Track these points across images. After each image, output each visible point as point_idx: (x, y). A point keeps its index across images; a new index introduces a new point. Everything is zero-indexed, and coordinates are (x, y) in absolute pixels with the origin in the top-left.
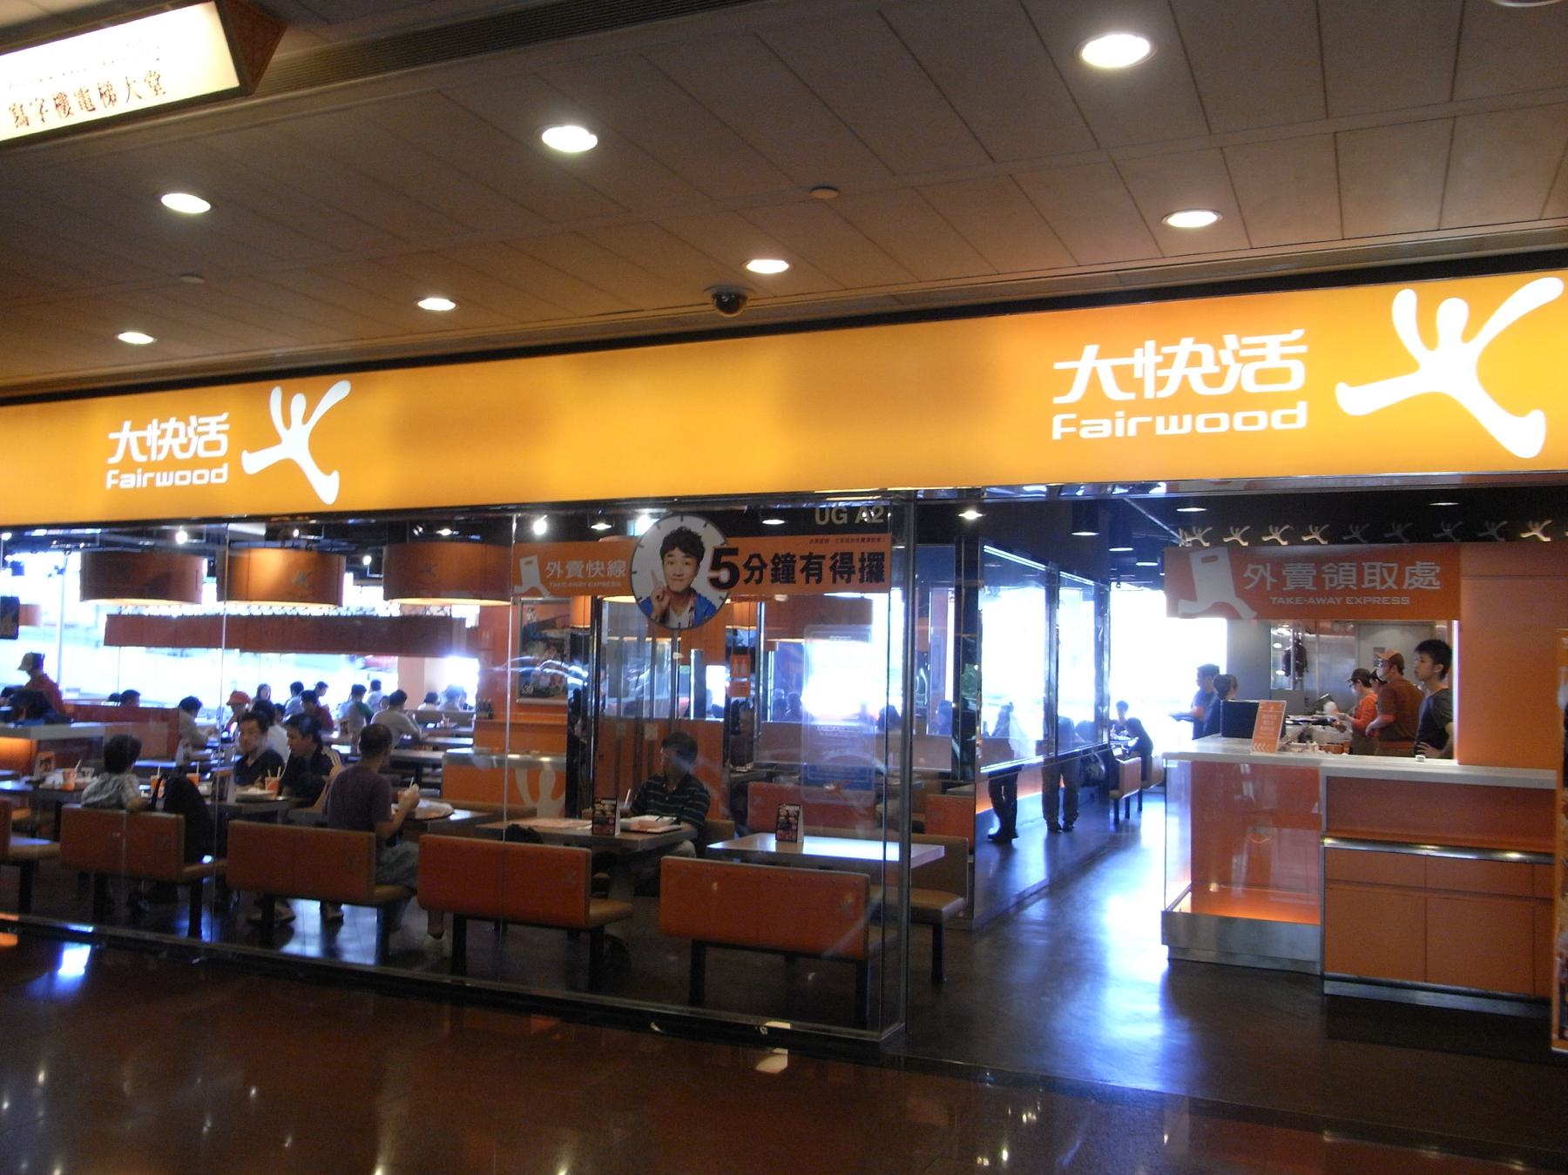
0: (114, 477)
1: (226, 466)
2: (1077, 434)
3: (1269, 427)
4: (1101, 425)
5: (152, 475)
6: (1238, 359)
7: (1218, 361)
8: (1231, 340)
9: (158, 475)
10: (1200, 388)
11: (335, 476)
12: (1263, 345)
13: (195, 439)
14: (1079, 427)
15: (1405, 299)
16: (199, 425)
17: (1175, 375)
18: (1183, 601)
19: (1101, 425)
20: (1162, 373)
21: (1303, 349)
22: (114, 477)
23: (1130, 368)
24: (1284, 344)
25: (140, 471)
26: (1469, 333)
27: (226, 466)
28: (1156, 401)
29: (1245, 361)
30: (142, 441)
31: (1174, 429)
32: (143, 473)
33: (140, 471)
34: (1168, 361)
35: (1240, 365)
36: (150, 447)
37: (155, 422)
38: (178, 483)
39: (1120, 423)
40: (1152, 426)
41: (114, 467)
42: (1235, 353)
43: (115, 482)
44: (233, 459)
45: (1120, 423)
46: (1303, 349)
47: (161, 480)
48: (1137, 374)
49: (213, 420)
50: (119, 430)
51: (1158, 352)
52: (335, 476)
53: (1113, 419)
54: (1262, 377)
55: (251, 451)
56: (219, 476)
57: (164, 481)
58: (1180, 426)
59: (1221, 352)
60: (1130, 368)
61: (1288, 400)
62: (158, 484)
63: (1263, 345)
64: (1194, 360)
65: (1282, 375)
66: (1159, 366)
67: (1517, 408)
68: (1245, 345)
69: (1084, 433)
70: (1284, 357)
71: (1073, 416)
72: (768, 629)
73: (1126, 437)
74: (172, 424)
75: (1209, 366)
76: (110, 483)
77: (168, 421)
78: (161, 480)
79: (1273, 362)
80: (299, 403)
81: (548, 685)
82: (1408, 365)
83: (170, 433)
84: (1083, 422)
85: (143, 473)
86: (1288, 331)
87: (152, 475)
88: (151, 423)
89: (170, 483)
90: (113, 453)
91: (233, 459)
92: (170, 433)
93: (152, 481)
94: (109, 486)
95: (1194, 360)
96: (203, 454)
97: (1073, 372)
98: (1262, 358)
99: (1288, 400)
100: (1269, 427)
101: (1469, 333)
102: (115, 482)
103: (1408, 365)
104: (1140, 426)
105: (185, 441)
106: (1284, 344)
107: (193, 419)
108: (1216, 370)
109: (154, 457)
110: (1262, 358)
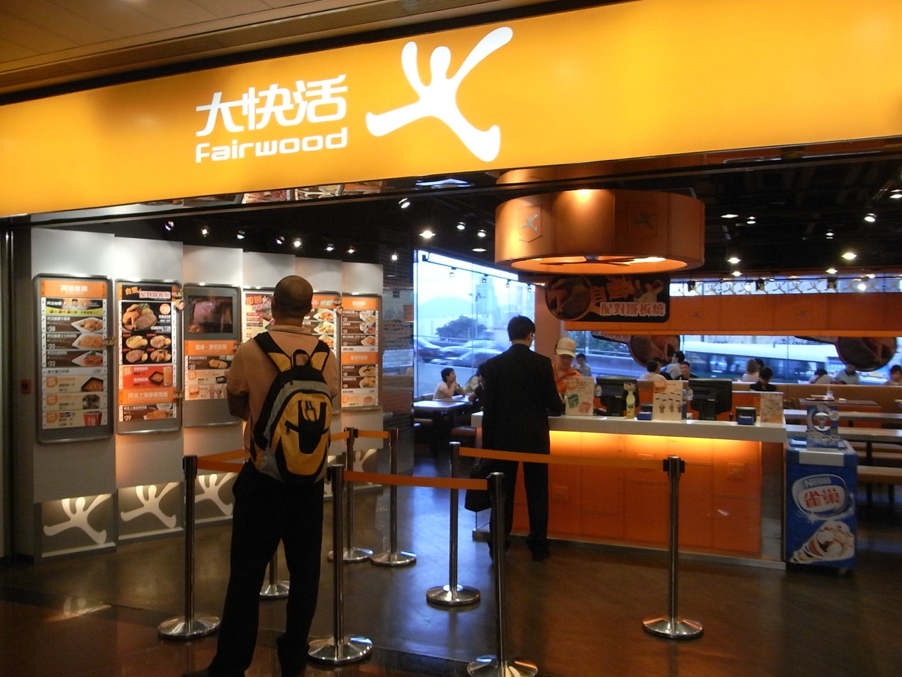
0: (204, 150)
1: (344, 131)
2: (209, 158)
3: (301, 150)
4: (224, 150)
5: (251, 145)
6: (305, 98)
7: (292, 101)
8: (300, 84)
9: (258, 145)
10: (283, 121)
11: (495, 131)
12: (320, 88)
13: (303, 105)
14: (212, 153)
15: (410, 49)
16: (308, 89)
17: (267, 111)
18: (511, 345)
19: (224, 150)
20: (259, 111)
21: (344, 89)
22: (204, 150)
23: (240, 108)
24: (333, 86)
25: (235, 142)
26: (451, 72)
27: (344, 131)
28: (256, 131)
29: (309, 99)
30: (236, 113)
31: (266, 152)
32: (239, 144)
33: (235, 142)
34: (262, 102)
35: (307, 102)
36: (247, 117)
37: (252, 90)
38: (283, 151)
39: (235, 148)
40: (253, 149)
41: (203, 140)
42: (303, 94)
43: (207, 155)
44: (355, 121)
45: (235, 148)
46: (344, 89)
47: (262, 151)
48: (245, 113)
49: (326, 84)
50: (209, 101)
51: (256, 96)
52: (495, 131)
53: (230, 145)
54: (320, 111)
55: (377, 112)
56: (337, 141)
57: (264, 150)
58: (270, 149)
59: (295, 94)
60: (240, 108)
61: (334, 127)
62: (258, 153)
63: (320, 88)
64: (279, 100)
65: (331, 109)
66: (258, 106)
67: (482, 124)
68: (309, 88)
69: (215, 158)
70: (333, 95)
71: (207, 145)
72: (411, 389)
73: (238, 160)
74: (274, 90)
75: (287, 105)
76: (199, 156)
77: (268, 89)
78: (262, 151)
79: (327, 100)
80: (441, 56)
81: (784, 563)
82: (411, 97)
83: (270, 101)
84: (214, 149)
85: (239, 144)
86: (336, 77)
87: (251, 145)
88: (247, 92)
89: (274, 152)
90: (203, 126)
91: (355, 121)
92: (270, 101)
93: (250, 152)
94: (198, 160)
95: (279, 100)
96: (313, 119)
97: (208, 112)
98: (319, 97)
99: (334, 127)
100: (301, 150)
101: (451, 73)
102: (207, 155)
103: (411, 97)
104: (247, 149)
105: (291, 107)
106: (333, 86)
107: (300, 84)
108: (291, 107)
109: (251, 127)
110: (319, 97)
